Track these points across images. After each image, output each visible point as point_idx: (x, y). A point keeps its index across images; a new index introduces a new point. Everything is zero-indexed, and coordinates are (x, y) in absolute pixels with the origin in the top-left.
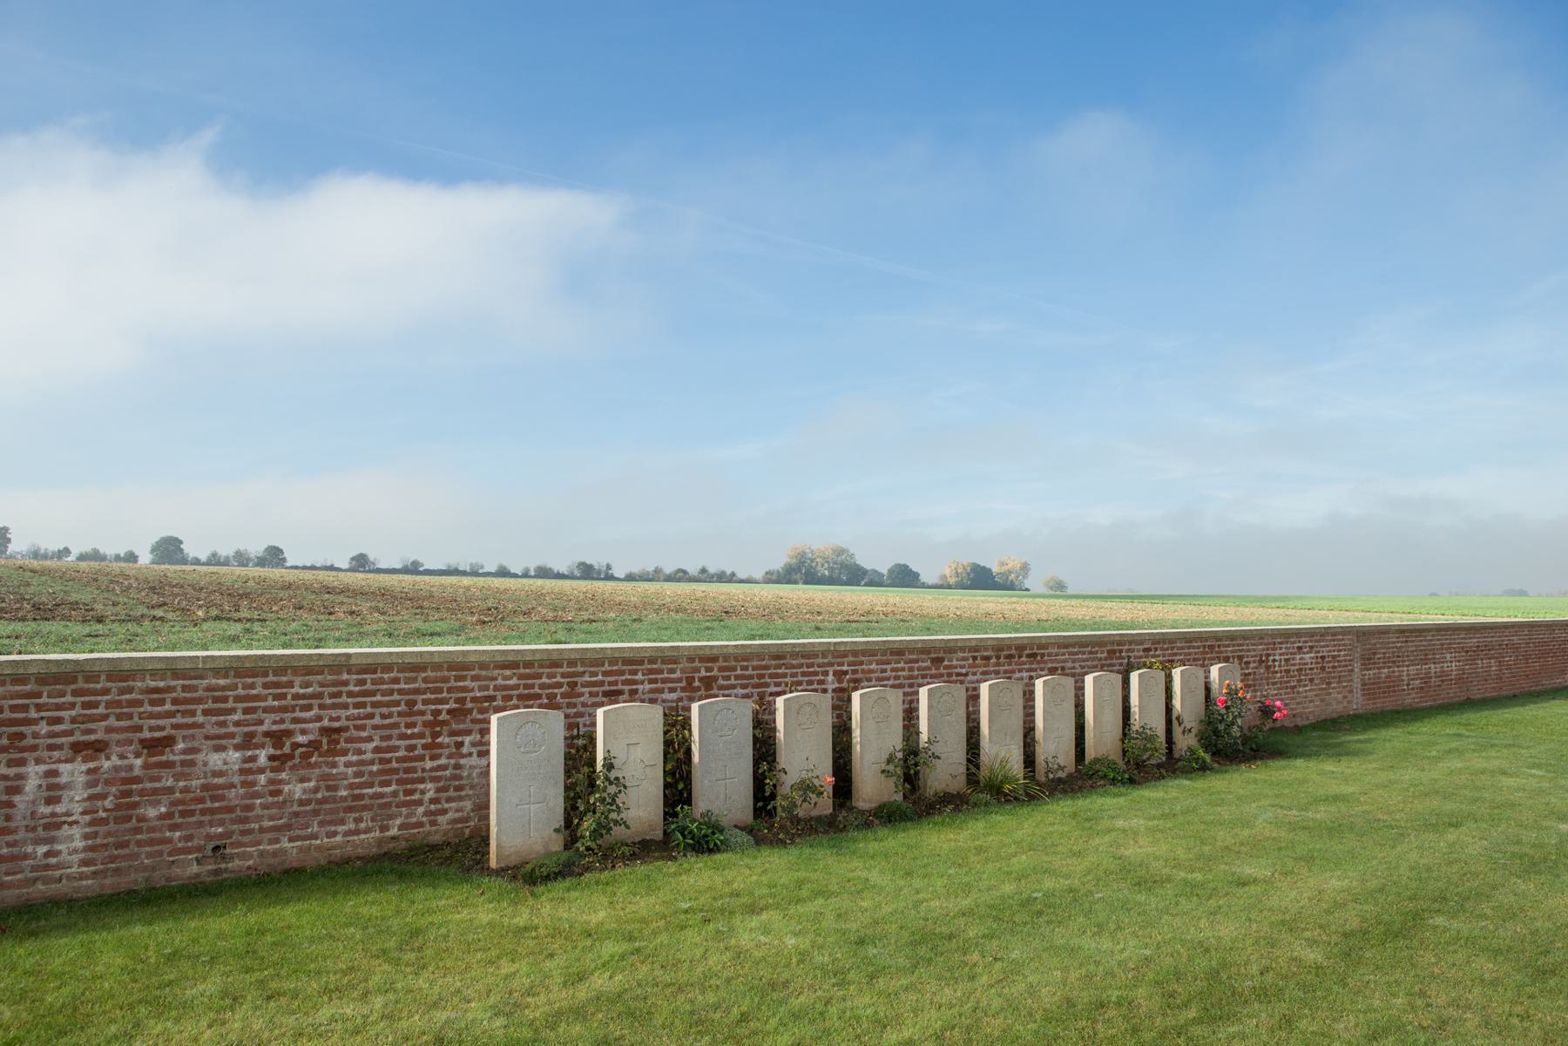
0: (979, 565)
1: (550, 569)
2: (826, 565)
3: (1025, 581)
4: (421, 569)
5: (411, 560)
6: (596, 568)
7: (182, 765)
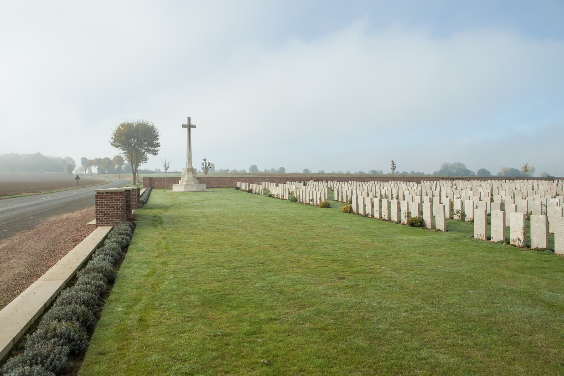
0: (514, 169)
1: (363, 172)
2: (455, 170)
3: (533, 175)
4: (324, 173)
5: (321, 170)
6: (378, 172)
7: (108, 220)
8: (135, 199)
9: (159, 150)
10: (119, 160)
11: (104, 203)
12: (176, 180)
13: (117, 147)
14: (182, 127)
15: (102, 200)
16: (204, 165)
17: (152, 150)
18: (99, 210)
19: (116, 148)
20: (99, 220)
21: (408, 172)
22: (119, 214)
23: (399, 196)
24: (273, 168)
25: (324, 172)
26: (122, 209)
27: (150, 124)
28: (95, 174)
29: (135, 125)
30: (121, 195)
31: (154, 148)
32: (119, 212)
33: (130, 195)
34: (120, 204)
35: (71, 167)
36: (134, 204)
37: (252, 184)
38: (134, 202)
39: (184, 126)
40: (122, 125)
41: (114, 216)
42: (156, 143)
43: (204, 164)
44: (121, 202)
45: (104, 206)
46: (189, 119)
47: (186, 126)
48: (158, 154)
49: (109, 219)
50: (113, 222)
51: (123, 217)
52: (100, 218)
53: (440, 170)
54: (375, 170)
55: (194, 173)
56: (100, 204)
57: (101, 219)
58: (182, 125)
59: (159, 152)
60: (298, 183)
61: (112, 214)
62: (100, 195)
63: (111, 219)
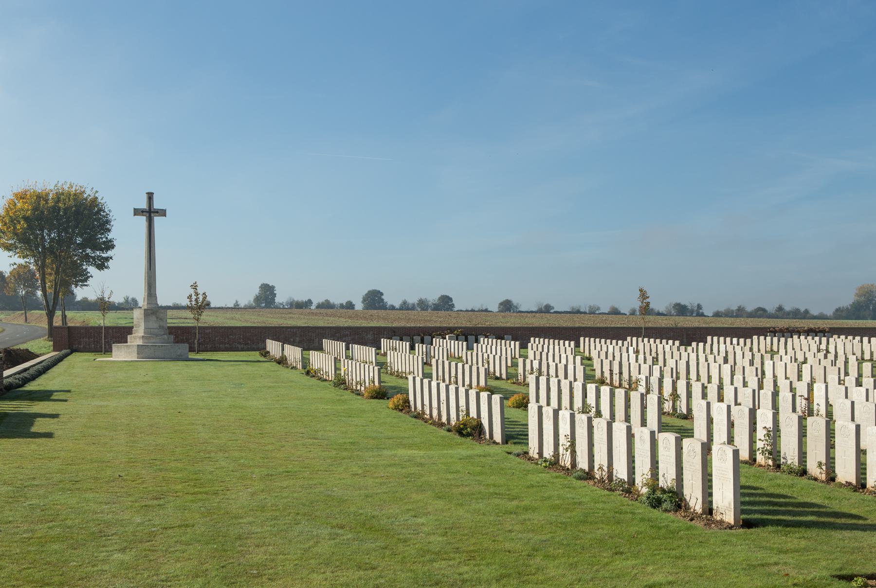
4: (552, 311)
9: (111, 258)
10: (22, 276)
12: (121, 334)
14: (135, 215)
16: (193, 300)
17: (94, 258)
21: (767, 309)
23: (665, 372)
24: (423, 298)
25: (553, 308)
27: (89, 193)
39: (137, 212)
40: (22, 196)
42: (104, 239)
43: (194, 297)
46: (150, 196)
48: (107, 267)
53: (853, 303)
54: (683, 303)
58: (135, 209)
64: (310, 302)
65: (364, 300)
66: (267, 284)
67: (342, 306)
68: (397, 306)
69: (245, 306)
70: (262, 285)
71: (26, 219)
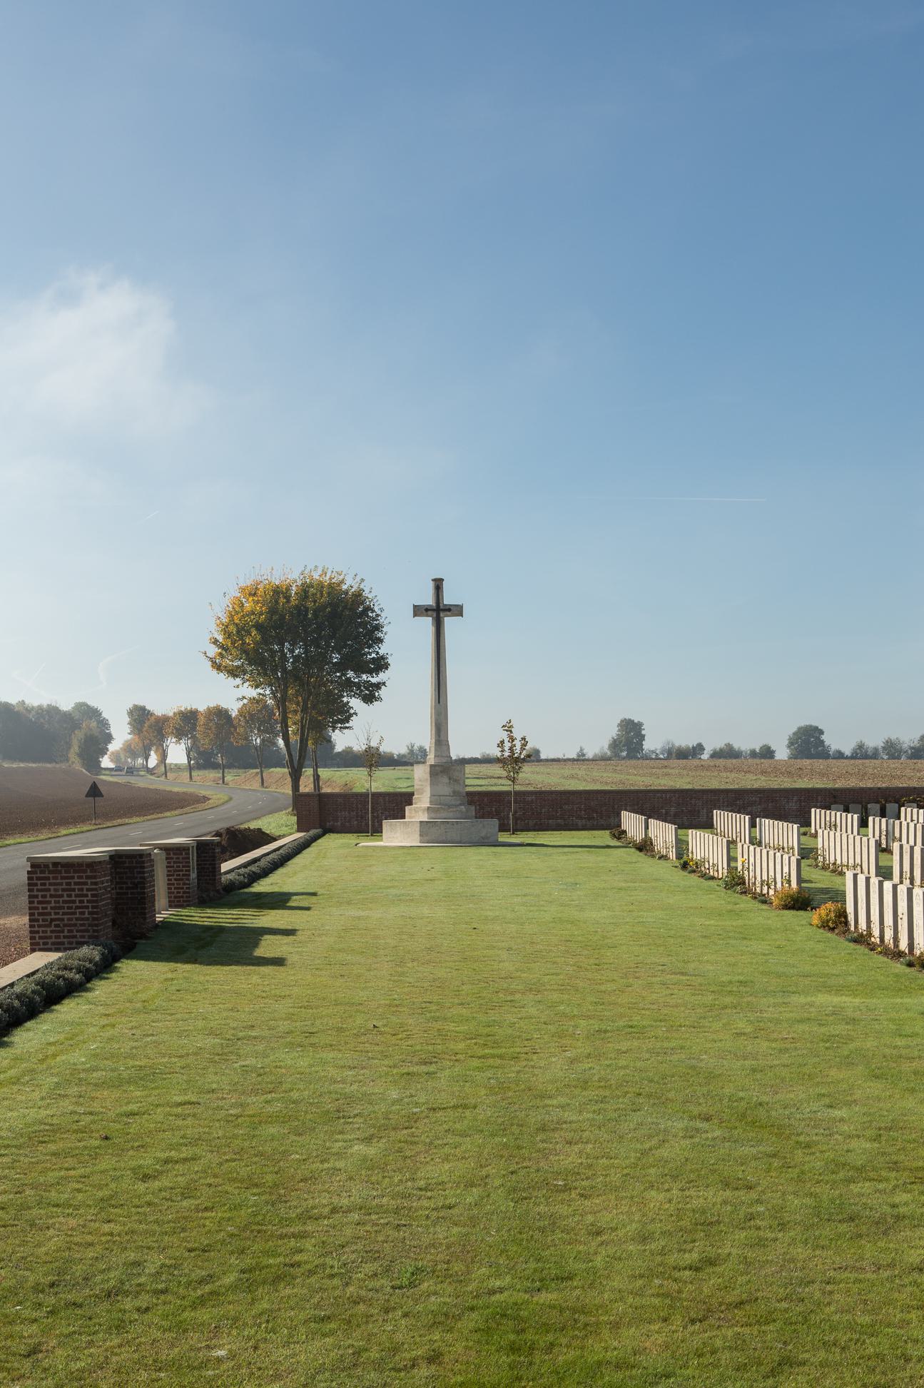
8: (186, 875)
11: (49, 890)
12: (396, 804)
13: (233, 673)
14: (415, 615)
15: (45, 884)
16: (506, 748)
17: (358, 685)
18: (38, 908)
19: (231, 679)
20: (37, 936)
22: (87, 919)
24: (893, 737)
26: (93, 907)
27: (350, 584)
28: (178, 768)
29: (294, 588)
30: (91, 872)
31: (364, 677)
32: (87, 915)
33: (144, 867)
34: (89, 893)
35: (98, 741)
36: (184, 893)
37: (767, 821)
38: (184, 884)
39: (419, 611)
41: (75, 925)
42: (374, 655)
43: (507, 745)
44: (92, 890)
45: (48, 899)
46: (438, 584)
47: (427, 610)
48: (379, 699)
49: (63, 932)
50: (71, 940)
51: (95, 928)
52: (41, 929)
55: (456, 781)
56: (40, 894)
57: (43, 932)
59: (383, 692)
60: (838, 814)
61: (69, 919)
62: (38, 870)
63: (66, 934)
64: (699, 748)
65: (791, 744)
66: (630, 720)
67: (753, 754)
68: (848, 752)
69: (596, 755)
70: (622, 721)
71: (259, 627)
